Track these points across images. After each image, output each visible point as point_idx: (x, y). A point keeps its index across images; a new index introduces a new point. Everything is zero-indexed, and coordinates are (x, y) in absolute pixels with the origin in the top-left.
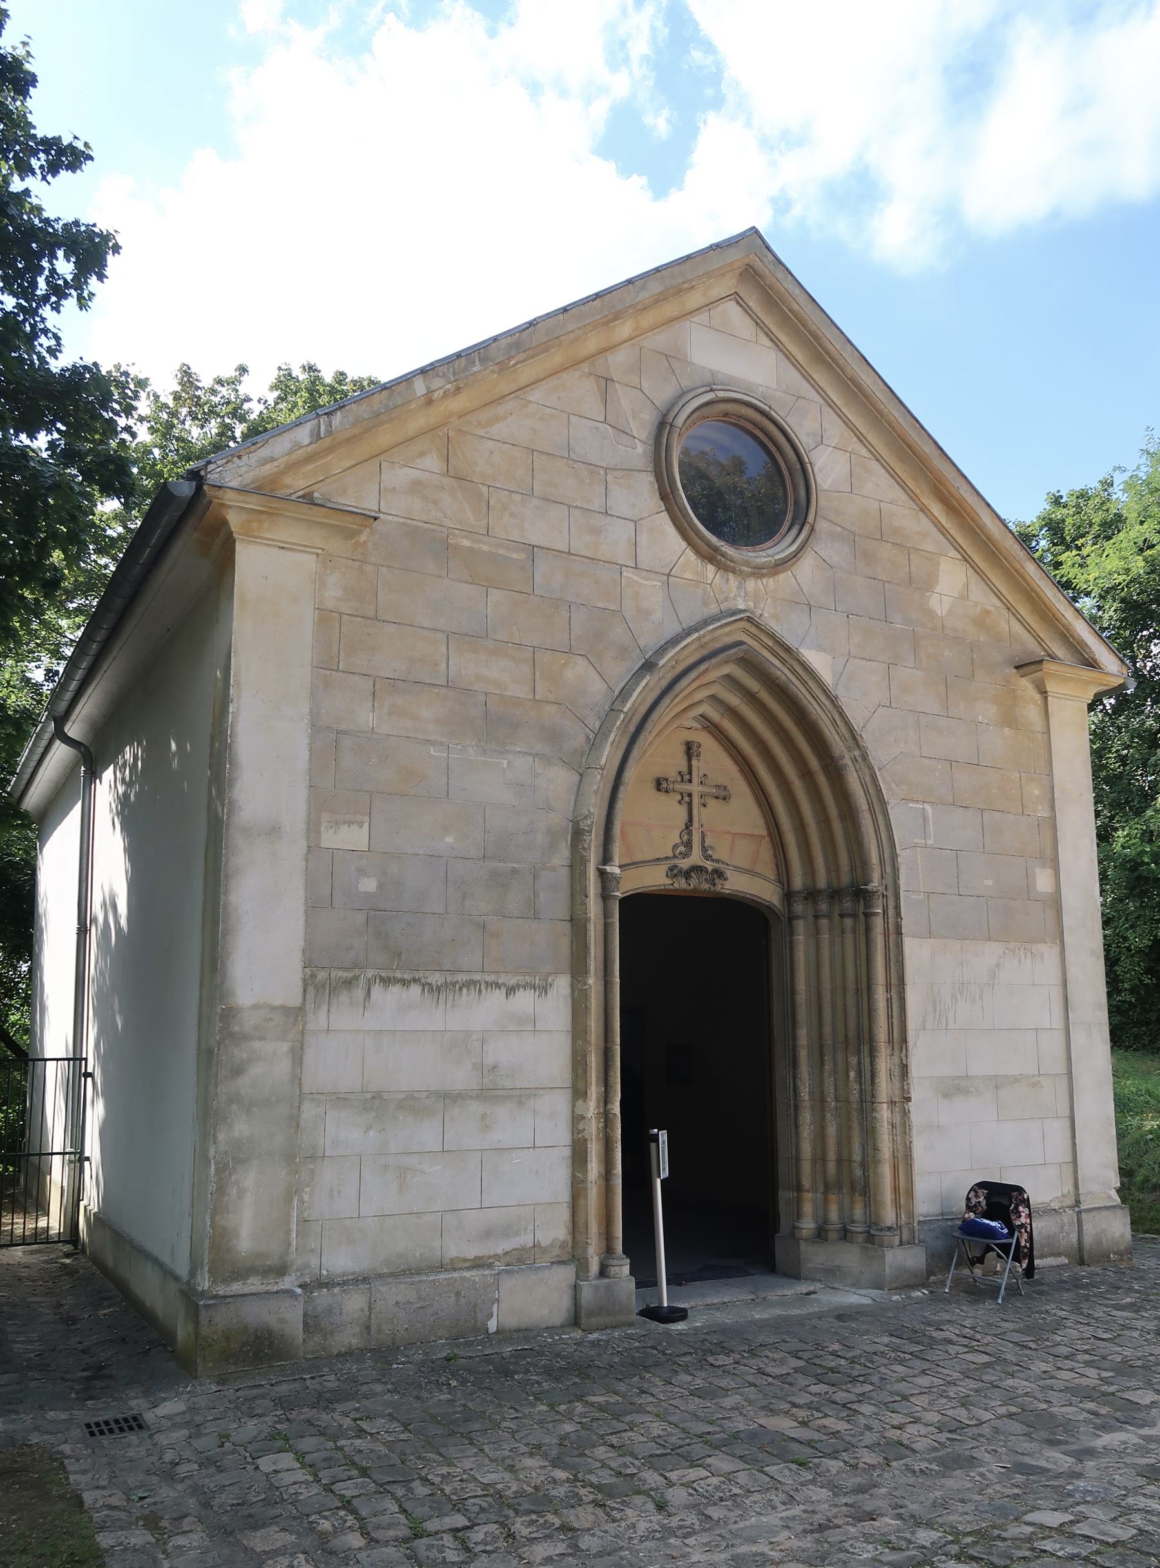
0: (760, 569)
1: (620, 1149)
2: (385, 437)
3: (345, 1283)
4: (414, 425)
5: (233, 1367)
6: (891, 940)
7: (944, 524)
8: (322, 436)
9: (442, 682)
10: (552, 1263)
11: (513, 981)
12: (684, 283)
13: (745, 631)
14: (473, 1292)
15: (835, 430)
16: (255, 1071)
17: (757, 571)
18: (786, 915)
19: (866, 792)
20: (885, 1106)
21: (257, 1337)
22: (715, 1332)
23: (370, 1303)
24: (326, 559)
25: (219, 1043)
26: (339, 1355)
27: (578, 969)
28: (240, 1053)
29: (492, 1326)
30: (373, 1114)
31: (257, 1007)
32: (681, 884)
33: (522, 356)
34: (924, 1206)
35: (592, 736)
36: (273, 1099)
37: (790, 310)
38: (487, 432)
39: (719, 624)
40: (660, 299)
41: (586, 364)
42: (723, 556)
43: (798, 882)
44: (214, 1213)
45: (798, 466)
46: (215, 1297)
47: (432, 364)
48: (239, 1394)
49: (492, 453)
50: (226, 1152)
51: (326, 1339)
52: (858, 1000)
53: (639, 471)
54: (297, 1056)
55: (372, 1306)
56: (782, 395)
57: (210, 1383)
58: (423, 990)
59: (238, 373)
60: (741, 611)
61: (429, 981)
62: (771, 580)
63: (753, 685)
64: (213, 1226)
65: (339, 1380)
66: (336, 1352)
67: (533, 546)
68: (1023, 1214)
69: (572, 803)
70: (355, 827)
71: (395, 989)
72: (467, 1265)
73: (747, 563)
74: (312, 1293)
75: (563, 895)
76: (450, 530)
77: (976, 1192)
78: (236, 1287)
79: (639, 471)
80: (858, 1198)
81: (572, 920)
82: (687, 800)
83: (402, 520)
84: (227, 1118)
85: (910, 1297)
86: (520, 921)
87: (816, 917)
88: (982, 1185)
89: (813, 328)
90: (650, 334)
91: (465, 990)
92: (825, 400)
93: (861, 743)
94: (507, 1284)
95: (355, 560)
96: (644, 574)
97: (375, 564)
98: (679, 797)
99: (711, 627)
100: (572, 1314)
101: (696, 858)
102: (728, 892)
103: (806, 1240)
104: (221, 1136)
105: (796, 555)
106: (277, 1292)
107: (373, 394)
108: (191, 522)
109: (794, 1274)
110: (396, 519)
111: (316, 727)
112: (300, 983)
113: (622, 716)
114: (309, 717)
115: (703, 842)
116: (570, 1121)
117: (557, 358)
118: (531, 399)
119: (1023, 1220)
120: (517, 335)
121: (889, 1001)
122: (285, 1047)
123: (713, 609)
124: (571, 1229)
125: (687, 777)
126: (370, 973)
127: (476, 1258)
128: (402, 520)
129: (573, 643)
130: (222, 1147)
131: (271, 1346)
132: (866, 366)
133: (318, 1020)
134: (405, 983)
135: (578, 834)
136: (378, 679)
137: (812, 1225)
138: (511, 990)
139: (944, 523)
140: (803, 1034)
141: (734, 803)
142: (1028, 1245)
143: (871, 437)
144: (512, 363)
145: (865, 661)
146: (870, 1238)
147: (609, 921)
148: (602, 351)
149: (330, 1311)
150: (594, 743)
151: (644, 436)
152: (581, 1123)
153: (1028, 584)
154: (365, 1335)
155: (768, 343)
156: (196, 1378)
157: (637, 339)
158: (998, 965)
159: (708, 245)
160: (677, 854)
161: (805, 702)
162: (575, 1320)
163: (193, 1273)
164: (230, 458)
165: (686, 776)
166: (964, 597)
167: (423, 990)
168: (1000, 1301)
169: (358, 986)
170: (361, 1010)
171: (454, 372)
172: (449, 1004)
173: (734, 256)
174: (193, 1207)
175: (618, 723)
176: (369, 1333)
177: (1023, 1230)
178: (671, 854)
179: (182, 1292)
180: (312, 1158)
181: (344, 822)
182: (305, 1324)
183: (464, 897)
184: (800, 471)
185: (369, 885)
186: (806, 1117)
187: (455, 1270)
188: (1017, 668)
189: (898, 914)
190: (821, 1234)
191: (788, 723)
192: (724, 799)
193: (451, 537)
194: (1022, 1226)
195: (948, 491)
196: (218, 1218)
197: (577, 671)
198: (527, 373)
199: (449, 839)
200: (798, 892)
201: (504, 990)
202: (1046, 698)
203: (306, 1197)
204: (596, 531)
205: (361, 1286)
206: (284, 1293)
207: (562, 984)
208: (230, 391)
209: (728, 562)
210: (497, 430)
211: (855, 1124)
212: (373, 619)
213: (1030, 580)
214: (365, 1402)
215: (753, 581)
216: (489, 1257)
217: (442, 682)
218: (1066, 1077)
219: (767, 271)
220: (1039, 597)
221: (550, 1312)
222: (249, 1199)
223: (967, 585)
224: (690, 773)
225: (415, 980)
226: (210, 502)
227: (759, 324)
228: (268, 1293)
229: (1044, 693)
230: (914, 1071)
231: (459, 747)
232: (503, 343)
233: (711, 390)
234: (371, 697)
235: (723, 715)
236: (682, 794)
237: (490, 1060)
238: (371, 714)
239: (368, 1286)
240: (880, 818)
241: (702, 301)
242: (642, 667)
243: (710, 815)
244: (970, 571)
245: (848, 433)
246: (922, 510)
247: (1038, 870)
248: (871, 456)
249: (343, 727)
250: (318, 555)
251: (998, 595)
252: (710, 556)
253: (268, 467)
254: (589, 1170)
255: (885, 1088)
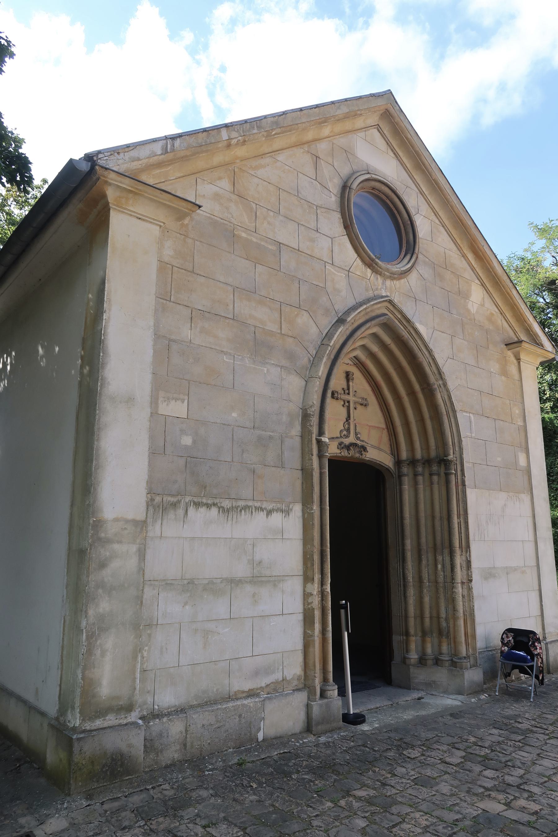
0: (394, 274)
1: (330, 614)
2: (200, 163)
3: (169, 714)
4: (218, 159)
5: (96, 784)
6: (459, 489)
7: (473, 265)
8: (169, 151)
9: (231, 316)
10: (293, 690)
11: (270, 507)
12: (358, 110)
13: (387, 308)
14: (249, 714)
15: (424, 208)
16: (115, 564)
17: (392, 275)
18: (397, 474)
19: (445, 404)
20: (460, 584)
21: (113, 759)
22: (391, 731)
23: (186, 728)
24: (164, 230)
25: (91, 545)
26: (167, 767)
27: (306, 501)
28: (104, 552)
29: (260, 736)
30: (189, 594)
31: (116, 520)
32: (345, 453)
33: (278, 130)
34: (480, 644)
35: (312, 359)
36: (126, 585)
37: (405, 136)
38: (255, 173)
39: (376, 302)
40: (347, 117)
41: (306, 146)
42: (376, 264)
43: (404, 455)
44: (85, 669)
45: (409, 222)
46: (84, 731)
47: (231, 123)
48: (106, 807)
49: (258, 185)
50: (94, 624)
51: (158, 756)
52: (441, 523)
53: (333, 210)
54: (142, 554)
55: (188, 729)
56: (400, 184)
57: (81, 800)
58: (219, 511)
59: (42, 183)
60: (382, 297)
61: (222, 505)
62: (398, 282)
63: (387, 339)
64: (83, 679)
65: (173, 788)
66: (164, 764)
67: (280, 243)
68: (538, 647)
69: (302, 398)
70: (179, 402)
71: (203, 510)
72: (244, 695)
73: (388, 270)
74: (149, 723)
75: (297, 454)
76: (235, 226)
77: (507, 635)
78: (98, 723)
79: (333, 210)
80: (444, 640)
81: (302, 470)
82: (347, 404)
83: (208, 215)
84: (95, 599)
85: (480, 699)
86: (273, 469)
87: (431, 475)
88: (510, 630)
89: (418, 149)
90: (338, 137)
91: (243, 512)
92: (419, 190)
93: (443, 377)
94: (269, 706)
95: (181, 234)
96: (337, 268)
97: (193, 239)
98: (343, 403)
99: (372, 303)
100: (306, 725)
101: (352, 439)
102: (368, 459)
103: (413, 665)
104: (91, 612)
105: (410, 270)
106: (126, 724)
107: (198, 133)
108: (80, 195)
109: (406, 686)
110: (205, 214)
111: (157, 336)
112: (145, 504)
113: (329, 348)
114: (153, 328)
115: (356, 429)
116: (302, 597)
117: (293, 138)
118: (279, 159)
119: (538, 651)
120: (277, 118)
121: (459, 524)
122: (134, 548)
123: (370, 294)
124: (303, 667)
125: (347, 391)
126: (188, 499)
127: (250, 690)
128: (208, 215)
129: (301, 303)
130: (91, 620)
131: (122, 765)
132: (441, 174)
133: (155, 530)
134: (208, 506)
135: (306, 417)
136: (194, 310)
137: (416, 657)
138: (269, 513)
139: (473, 264)
140: (408, 544)
141: (370, 408)
142: (542, 665)
143: (441, 213)
144: (273, 133)
145: (441, 333)
146: (454, 664)
147: (323, 471)
148: (315, 140)
149: (161, 735)
150: (314, 362)
151: (335, 192)
152: (310, 599)
153: (513, 301)
154: (183, 750)
155: (393, 155)
156: (69, 795)
157: (331, 138)
158: (505, 505)
159: (369, 93)
160: (342, 435)
161: (417, 351)
162: (309, 728)
163: (62, 711)
164: (112, 153)
165: (347, 391)
166: (482, 305)
167: (219, 511)
168: (532, 700)
169: (180, 507)
170: (182, 523)
171: (243, 130)
172: (234, 522)
173: (381, 102)
174: (62, 663)
175: (328, 352)
176: (185, 749)
177: (539, 657)
178: (339, 436)
179: (51, 726)
180: (150, 626)
181: (173, 399)
182: (145, 746)
183: (243, 451)
184: (410, 225)
185: (187, 440)
186: (411, 592)
187: (237, 699)
188: (506, 345)
189: (463, 474)
190: (422, 661)
191: (404, 363)
192: (366, 406)
193: (236, 230)
194: (538, 654)
195: (478, 247)
196: (87, 672)
197: (303, 319)
198: (278, 143)
199: (234, 415)
200: (405, 461)
201: (265, 512)
202: (519, 363)
203: (145, 654)
204: (312, 240)
205: (180, 716)
206: (131, 724)
207: (297, 509)
208: (37, 192)
209: (379, 268)
210: (261, 173)
211: (442, 596)
212: (191, 272)
213: (514, 299)
214: (200, 807)
215: (389, 281)
216: (257, 689)
217: (231, 316)
218: (536, 568)
219: (396, 115)
220: (518, 309)
221: (294, 724)
222: (108, 657)
223: (483, 299)
224: (348, 389)
225: (214, 505)
226: (98, 179)
227: (388, 143)
228: (120, 725)
229: (518, 360)
230: (474, 565)
231: (240, 357)
232: (270, 120)
233: (368, 173)
234: (190, 320)
235: (366, 357)
236: (344, 401)
237: (257, 558)
238: (190, 331)
239: (185, 715)
240: (452, 420)
241: (363, 125)
242: (337, 321)
243: (358, 414)
244: (485, 292)
245: (430, 210)
246: (463, 256)
247: (520, 454)
248: (440, 224)
249: (173, 337)
250: (160, 226)
251: (497, 306)
252: (370, 264)
253: (135, 163)
254: (316, 629)
255: (459, 575)
